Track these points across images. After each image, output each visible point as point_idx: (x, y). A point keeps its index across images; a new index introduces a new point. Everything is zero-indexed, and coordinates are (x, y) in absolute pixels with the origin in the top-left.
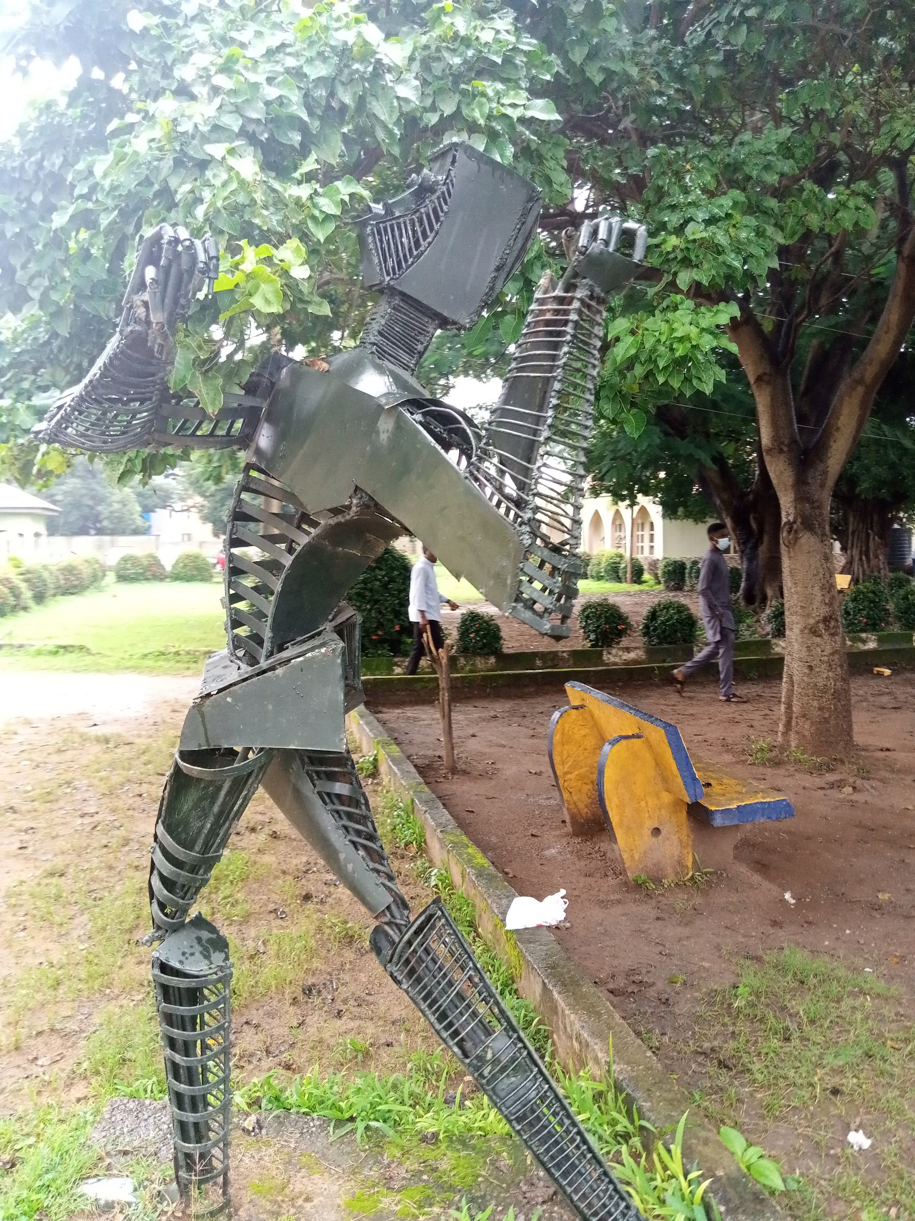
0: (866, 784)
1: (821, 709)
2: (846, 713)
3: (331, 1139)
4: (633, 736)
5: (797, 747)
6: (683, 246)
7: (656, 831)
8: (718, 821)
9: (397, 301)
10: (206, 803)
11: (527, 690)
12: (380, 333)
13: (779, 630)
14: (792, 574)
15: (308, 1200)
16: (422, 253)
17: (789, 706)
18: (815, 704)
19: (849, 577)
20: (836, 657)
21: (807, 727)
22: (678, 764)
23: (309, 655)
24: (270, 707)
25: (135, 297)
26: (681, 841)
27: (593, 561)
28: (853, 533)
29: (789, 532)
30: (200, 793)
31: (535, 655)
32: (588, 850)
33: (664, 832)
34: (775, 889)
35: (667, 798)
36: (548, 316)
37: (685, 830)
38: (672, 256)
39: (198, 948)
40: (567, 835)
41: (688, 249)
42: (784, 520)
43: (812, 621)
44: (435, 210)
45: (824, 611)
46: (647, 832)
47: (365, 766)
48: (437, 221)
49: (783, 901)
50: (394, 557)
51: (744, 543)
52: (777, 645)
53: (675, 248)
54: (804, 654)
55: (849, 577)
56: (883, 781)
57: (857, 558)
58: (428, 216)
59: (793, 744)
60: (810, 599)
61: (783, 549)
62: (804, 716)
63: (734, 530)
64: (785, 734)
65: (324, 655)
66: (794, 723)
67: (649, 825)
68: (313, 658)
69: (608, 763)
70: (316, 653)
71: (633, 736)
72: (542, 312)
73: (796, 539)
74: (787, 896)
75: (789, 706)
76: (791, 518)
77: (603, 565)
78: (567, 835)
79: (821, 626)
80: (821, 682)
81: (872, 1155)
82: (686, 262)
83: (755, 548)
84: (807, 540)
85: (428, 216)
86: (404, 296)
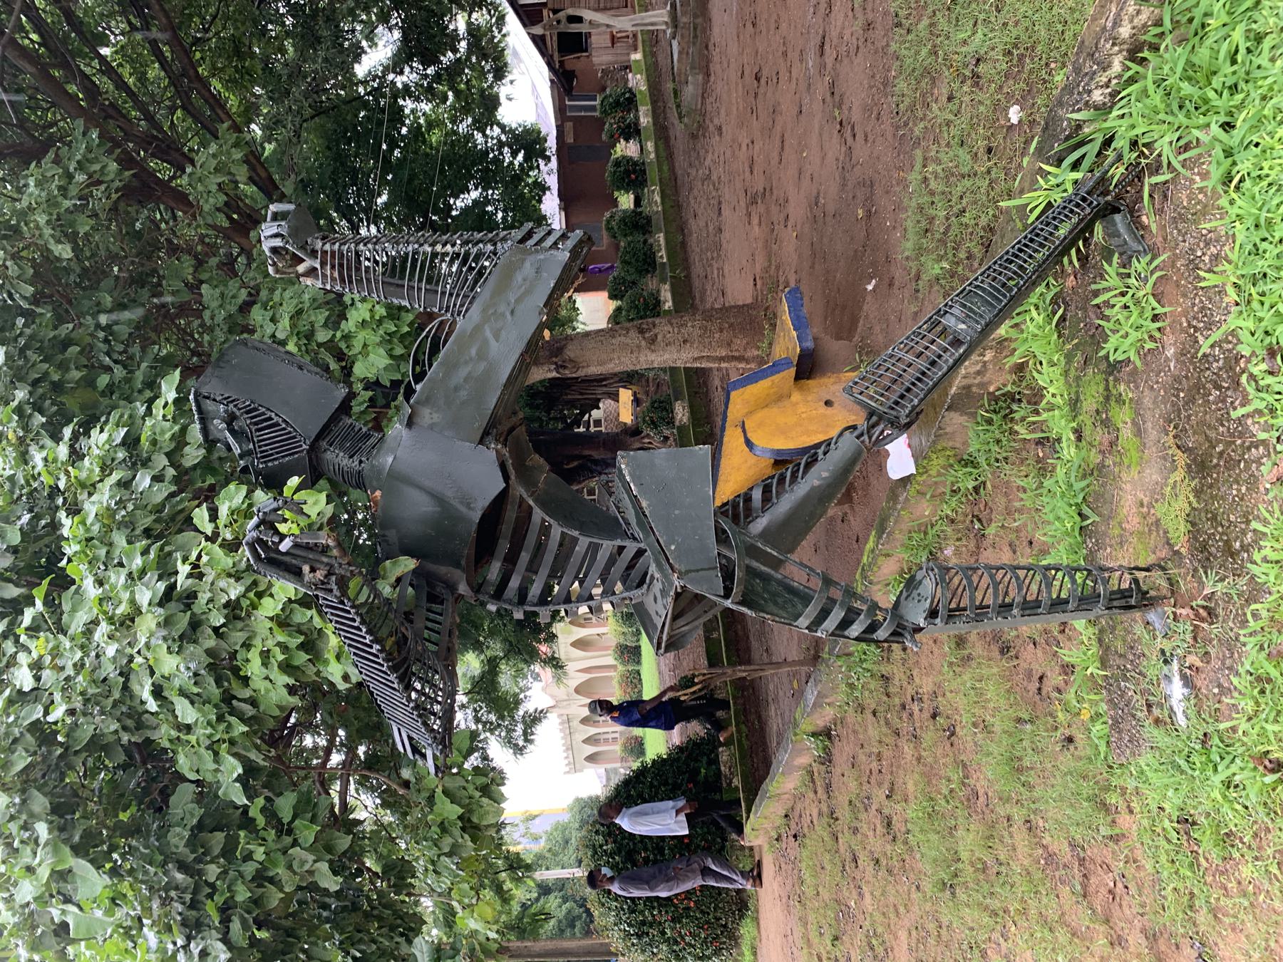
0: (782, 279)
1: (721, 330)
2: (725, 310)
3: (1097, 519)
4: (744, 431)
5: (758, 348)
6: (295, 339)
7: (828, 403)
8: (809, 344)
9: (324, 444)
10: (780, 600)
11: (740, 633)
12: (351, 457)
13: (668, 423)
14: (601, 363)
15: (1142, 505)
16: (284, 421)
17: (722, 359)
18: (717, 336)
19: (621, 390)
20: (674, 321)
21: (739, 342)
22: (762, 379)
23: (628, 478)
24: (677, 512)
25: (307, 579)
26: (835, 383)
27: (622, 641)
28: (582, 394)
29: (565, 367)
30: (770, 604)
31: (707, 639)
32: (861, 481)
33: (828, 398)
34: (869, 298)
35: (796, 396)
36: (336, 275)
37: (824, 380)
38: (303, 348)
39: (915, 593)
40: (852, 508)
41: (298, 334)
42: (554, 374)
43: (643, 343)
44: (247, 413)
45: (633, 334)
46: (829, 411)
47: (820, 745)
48: (256, 409)
49: (874, 290)
50: (616, 796)
51: (592, 472)
52: (681, 420)
53: (296, 344)
54: (673, 348)
55: (621, 390)
56: (778, 268)
57: (605, 389)
58: (252, 418)
59: (756, 353)
60: (624, 347)
61: (581, 373)
62: (729, 345)
63: (580, 483)
64: (748, 362)
65: (627, 465)
66: (736, 354)
67: (823, 409)
68: (630, 474)
69: (770, 447)
70: (626, 472)
71: (744, 431)
72: (333, 279)
73: (571, 360)
74: (870, 287)
75: (722, 359)
76: (553, 367)
77: (625, 630)
78: (852, 508)
79: (647, 335)
80: (698, 332)
81: (1021, 102)
82: (310, 336)
83: (596, 462)
84: (571, 352)
85: (252, 418)
86: (320, 436)
